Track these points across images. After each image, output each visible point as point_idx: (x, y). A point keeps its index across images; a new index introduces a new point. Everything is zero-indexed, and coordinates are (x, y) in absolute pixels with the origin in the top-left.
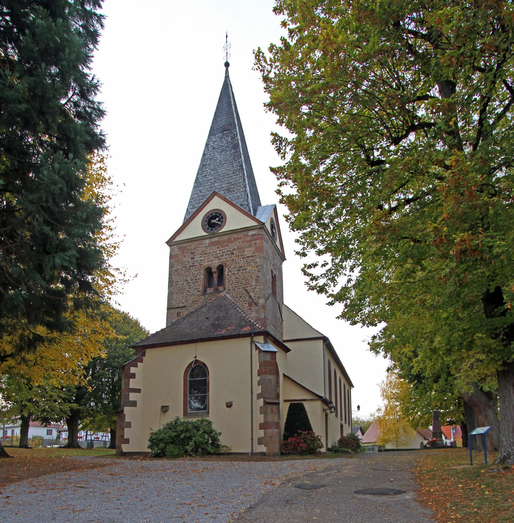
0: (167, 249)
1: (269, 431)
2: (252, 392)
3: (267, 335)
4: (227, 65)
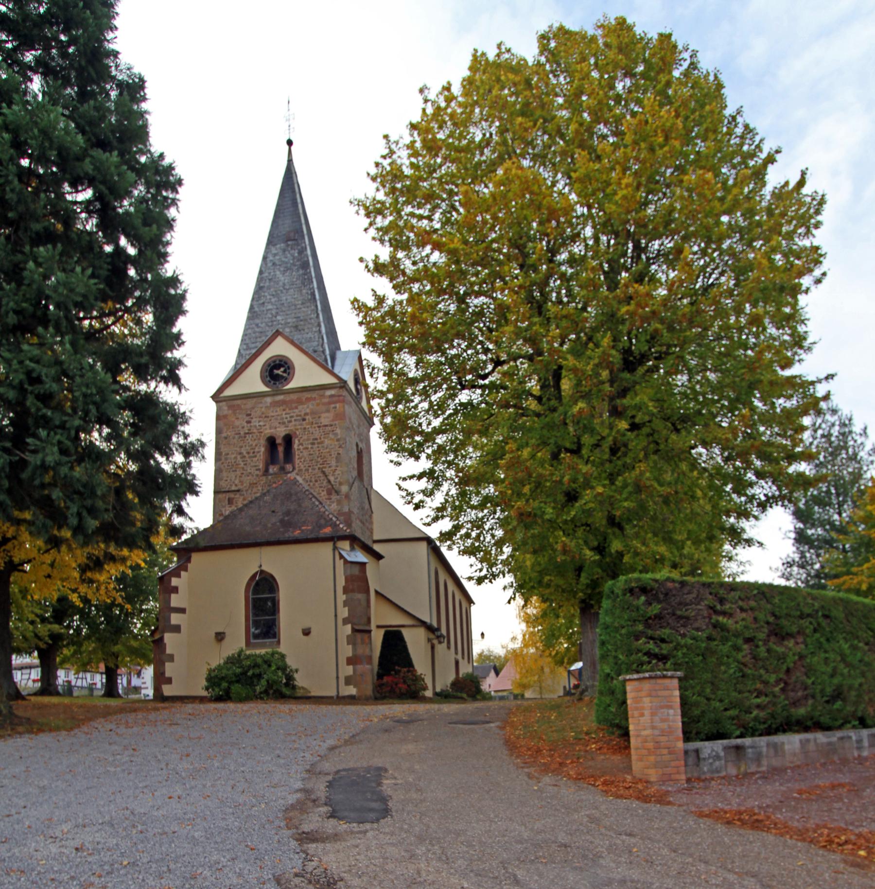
0: (213, 406)
1: (359, 667)
2: (336, 616)
3: (355, 541)
4: (290, 143)
